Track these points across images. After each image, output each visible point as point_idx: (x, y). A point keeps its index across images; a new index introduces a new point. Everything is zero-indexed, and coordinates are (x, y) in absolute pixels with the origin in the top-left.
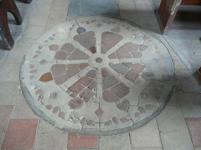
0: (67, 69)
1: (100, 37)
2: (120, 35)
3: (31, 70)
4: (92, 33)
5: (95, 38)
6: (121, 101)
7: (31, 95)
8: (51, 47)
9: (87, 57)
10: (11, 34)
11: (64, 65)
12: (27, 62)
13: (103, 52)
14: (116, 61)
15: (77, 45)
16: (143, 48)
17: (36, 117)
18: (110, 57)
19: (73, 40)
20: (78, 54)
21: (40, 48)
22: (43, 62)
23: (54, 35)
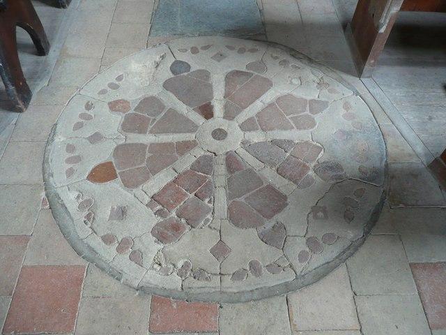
0: (148, 155)
1: (223, 83)
2: (265, 79)
3: (68, 155)
4: (205, 75)
5: (211, 86)
6: (269, 225)
7: (68, 213)
8: (113, 106)
9: (193, 128)
10: (25, 77)
11: (143, 146)
12: (59, 139)
13: (229, 116)
14: (256, 137)
15: (172, 101)
16: (317, 106)
17: (80, 261)
18: (245, 127)
19: (161, 89)
20: (173, 121)
21: (88, 107)
22: (96, 138)
23: (119, 78)
